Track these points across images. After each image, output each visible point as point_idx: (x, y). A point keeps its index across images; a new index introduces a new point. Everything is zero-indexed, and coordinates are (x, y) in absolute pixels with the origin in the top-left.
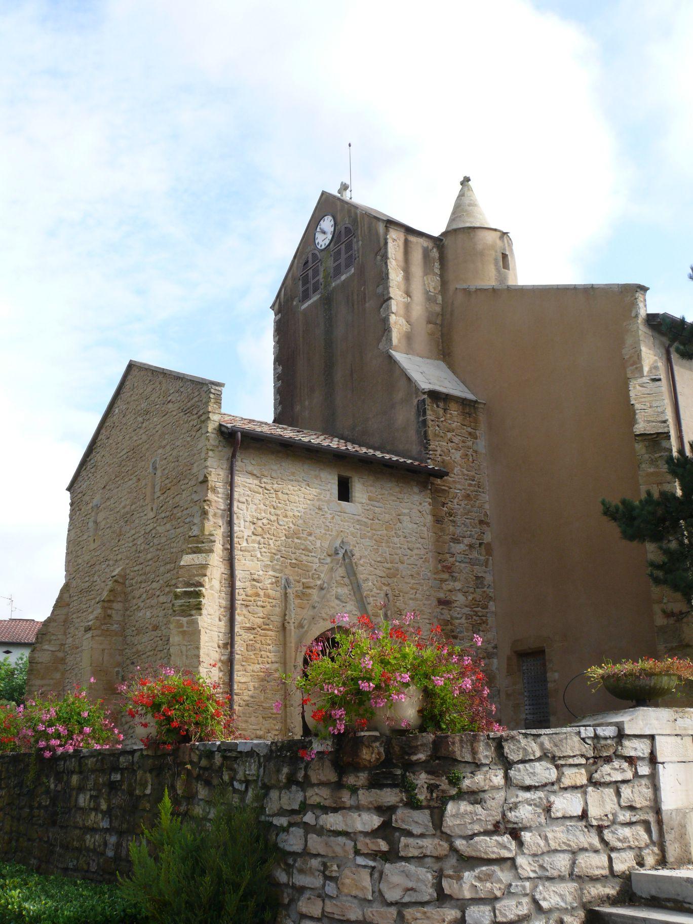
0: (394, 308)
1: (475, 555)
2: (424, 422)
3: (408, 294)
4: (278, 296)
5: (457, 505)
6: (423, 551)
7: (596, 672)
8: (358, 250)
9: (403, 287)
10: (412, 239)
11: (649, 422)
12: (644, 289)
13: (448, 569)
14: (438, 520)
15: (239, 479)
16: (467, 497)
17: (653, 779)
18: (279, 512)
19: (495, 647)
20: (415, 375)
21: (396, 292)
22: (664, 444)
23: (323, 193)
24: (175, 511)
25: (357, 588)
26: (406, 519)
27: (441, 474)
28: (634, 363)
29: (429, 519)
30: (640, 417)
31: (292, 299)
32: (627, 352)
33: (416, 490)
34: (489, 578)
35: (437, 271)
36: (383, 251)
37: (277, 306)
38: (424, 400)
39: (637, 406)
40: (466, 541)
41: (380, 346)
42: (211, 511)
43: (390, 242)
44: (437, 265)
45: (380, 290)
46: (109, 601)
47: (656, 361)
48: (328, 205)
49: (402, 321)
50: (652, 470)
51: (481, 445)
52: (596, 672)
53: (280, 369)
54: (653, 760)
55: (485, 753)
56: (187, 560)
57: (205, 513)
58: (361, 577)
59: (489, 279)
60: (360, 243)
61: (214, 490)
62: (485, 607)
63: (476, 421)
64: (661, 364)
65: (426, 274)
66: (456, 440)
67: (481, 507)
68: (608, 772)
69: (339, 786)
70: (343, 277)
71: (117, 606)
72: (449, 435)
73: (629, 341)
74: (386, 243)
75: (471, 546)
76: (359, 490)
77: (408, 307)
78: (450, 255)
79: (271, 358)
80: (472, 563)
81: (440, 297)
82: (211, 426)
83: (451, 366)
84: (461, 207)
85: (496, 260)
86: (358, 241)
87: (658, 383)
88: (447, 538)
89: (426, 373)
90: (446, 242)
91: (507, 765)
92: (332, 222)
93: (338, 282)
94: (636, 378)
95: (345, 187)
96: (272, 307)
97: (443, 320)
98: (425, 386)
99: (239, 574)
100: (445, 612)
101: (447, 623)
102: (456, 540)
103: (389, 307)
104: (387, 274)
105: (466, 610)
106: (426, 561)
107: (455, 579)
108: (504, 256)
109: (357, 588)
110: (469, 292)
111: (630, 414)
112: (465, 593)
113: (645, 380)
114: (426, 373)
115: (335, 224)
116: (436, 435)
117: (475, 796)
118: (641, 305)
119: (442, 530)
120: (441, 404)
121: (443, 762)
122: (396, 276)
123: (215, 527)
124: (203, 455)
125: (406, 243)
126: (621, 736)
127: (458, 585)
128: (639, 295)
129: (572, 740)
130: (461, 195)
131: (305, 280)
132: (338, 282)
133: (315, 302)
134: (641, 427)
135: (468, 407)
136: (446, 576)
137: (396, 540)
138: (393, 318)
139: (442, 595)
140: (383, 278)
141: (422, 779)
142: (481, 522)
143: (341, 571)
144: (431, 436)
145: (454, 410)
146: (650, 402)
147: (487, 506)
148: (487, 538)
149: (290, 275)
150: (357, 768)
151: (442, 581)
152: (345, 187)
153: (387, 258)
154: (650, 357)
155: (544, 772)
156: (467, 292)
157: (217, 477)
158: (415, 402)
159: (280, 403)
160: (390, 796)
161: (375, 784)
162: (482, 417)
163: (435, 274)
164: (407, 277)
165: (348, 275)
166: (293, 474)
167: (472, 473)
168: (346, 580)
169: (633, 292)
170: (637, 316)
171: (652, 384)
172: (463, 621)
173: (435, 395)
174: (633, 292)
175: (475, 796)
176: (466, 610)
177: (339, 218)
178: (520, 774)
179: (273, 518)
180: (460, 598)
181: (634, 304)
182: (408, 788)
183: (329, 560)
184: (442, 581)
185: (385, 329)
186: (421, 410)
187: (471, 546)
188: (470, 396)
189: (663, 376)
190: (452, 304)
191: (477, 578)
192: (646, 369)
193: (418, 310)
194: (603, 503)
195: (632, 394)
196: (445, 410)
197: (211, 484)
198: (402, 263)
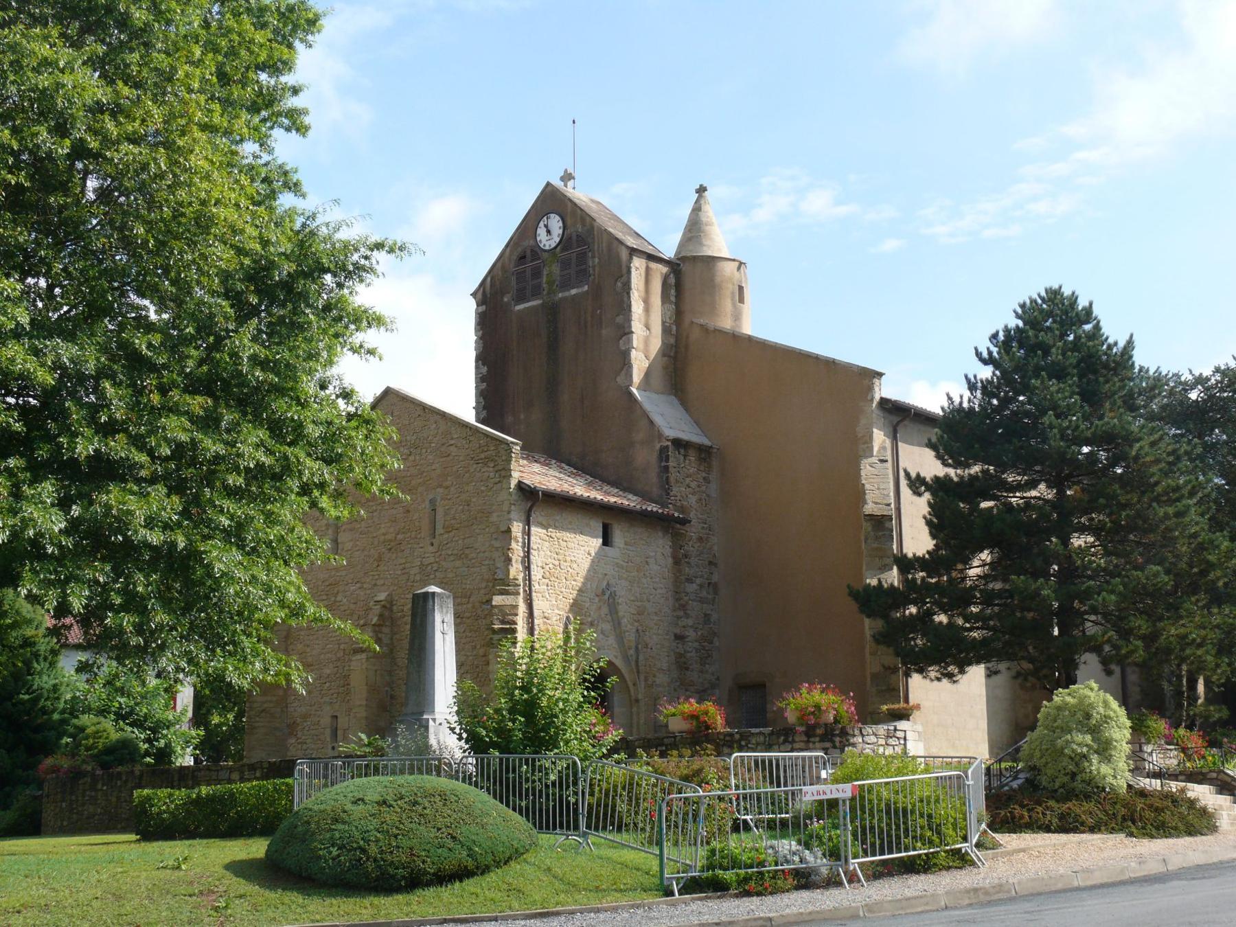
0: (635, 344)
1: (704, 594)
2: (666, 469)
3: (648, 327)
4: (483, 283)
5: (692, 547)
6: (664, 591)
7: (885, 707)
8: (594, 267)
9: (643, 320)
10: (653, 265)
11: (876, 503)
12: (880, 375)
13: (683, 607)
14: (677, 562)
15: (534, 529)
16: (700, 539)
17: (905, 745)
18: (560, 557)
19: (718, 679)
20: (658, 420)
21: (637, 326)
22: (887, 525)
23: (548, 184)
24: (467, 551)
25: (617, 624)
26: (651, 561)
27: (684, 522)
28: (866, 443)
29: (670, 560)
30: (869, 497)
31: (503, 294)
32: (860, 431)
33: (660, 534)
34: (715, 617)
35: (673, 299)
36: (624, 279)
37: (480, 295)
38: (667, 447)
39: (867, 486)
40: (698, 581)
41: (618, 379)
42: (514, 558)
43: (633, 270)
44: (673, 292)
45: (619, 319)
46: (379, 625)
47: (884, 441)
48: (552, 201)
49: (641, 356)
50: (875, 545)
51: (713, 489)
52: (885, 707)
53: (484, 370)
54: (905, 739)
55: (857, 732)
56: (498, 600)
57: (510, 560)
58: (621, 614)
59: (726, 324)
60: (597, 260)
61: (1183, 791)
62: (711, 642)
63: (710, 467)
64: (888, 443)
65: (663, 303)
66: (693, 485)
67: (711, 548)
68: (891, 741)
69: (808, 741)
70: (574, 292)
71: (386, 630)
72: (688, 480)
73: (863, 421)
74: (629, 272)
75: (701, 586)
76: (618, 536)
77: (647, 341)
78: (688, 283)
79: (472, 355)
80: (702, 601)
81: (674, 328)
82: (513, 483)
83: (684, 403)
84: (695, 228)
85: (733, 293)
86: (593, 257)
87: (885, 464)
88: (683, 578)
89: (670, 420)
90: (685, 268)
91: (863, 736)
92: (561, 224)
93: (567, 294)
94: (866, 457)
95: (567, 177)
96: (474, 295)
97: (676, 352)
98: (671, 433)
99: (536, 613)
100: (680, 646)
101: (680, 656)
102: (690, 581)
103: (630, 341)
104: (630, 306)
105: (696, 645)
106: (667, 599)
107: (687, 616)
108: (741, 288)
109: (617, 624)
110: (707, 330)
111: (859, 494)
112: (696, 630)
113: (874, 460)
114: (670, 420)
115: (565, 227)
116: (677, 481)
117: (854, 745)
118: (877, 389)
119: (680, 571)
120: (682, 451)
121: (844, 733)
122: (637, 308)
123: (516, 570)
124: (505, 508)
125: (648, 269)
126: (895, 730)
127: (690, 622)
128: (876, 381)
129: (882, 729)
130: (697, 209)
131: (520, 276)
132: (567, 294)
133: (533, 307)
134: (870, 508)
135: (704, 453)
136: (681, 613)
137: (644, 580)
138: (634, 353)
139: (678, 631)
140: (626, 309)
141: (837, 739)
142: (710, 563)
143: (605, 610)
144: (672, 480)
145: (692, 452)
146: (878, 483)
147: (715, 548)
148: (715, 578)
149: (499, 265)
150: (815, 736)
151: (678, 618)
152: (567, 177)
153: (630, 289)
154: (879, 438)
155: (873, 739)
156: (705, 329)
157: (517, 528)
158: (658, 446)
159: (484, 408)
160: (827, 745)
161: (821, 741)
162: (715, 463)
163: (671, 302)
164: (647, 310)
165: (580, 290)
166: (570, 523)
167: (705, 516)
168: (609, 618)
169: (870, 376)
170: (872, 400)
171: (880, 464)
172: (693, 654)
173: (678, 443)
174: (870, 376)
175: (854, 745)
176: (696, 645)
177: (569, 222)
178: (866, 739)
179: (557, 563)
180: (691, 634)
181: (870, 389)
182: (833, 742)
183: (597, 599)
184: (678, 618)
185: (625, 362)
186: (663, 454)
187: (701, 586)
188: (706, 442)
189: (889, 458)
190: (687, 337)
191: (706, 615)
192: (876, 449)
193: (656, 344)
194: (848, 586)
195: (863, 473)
196: (685, 456)
197: (513, 534)
198: (643, 294)
